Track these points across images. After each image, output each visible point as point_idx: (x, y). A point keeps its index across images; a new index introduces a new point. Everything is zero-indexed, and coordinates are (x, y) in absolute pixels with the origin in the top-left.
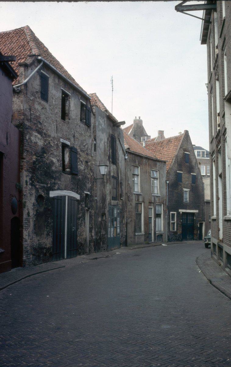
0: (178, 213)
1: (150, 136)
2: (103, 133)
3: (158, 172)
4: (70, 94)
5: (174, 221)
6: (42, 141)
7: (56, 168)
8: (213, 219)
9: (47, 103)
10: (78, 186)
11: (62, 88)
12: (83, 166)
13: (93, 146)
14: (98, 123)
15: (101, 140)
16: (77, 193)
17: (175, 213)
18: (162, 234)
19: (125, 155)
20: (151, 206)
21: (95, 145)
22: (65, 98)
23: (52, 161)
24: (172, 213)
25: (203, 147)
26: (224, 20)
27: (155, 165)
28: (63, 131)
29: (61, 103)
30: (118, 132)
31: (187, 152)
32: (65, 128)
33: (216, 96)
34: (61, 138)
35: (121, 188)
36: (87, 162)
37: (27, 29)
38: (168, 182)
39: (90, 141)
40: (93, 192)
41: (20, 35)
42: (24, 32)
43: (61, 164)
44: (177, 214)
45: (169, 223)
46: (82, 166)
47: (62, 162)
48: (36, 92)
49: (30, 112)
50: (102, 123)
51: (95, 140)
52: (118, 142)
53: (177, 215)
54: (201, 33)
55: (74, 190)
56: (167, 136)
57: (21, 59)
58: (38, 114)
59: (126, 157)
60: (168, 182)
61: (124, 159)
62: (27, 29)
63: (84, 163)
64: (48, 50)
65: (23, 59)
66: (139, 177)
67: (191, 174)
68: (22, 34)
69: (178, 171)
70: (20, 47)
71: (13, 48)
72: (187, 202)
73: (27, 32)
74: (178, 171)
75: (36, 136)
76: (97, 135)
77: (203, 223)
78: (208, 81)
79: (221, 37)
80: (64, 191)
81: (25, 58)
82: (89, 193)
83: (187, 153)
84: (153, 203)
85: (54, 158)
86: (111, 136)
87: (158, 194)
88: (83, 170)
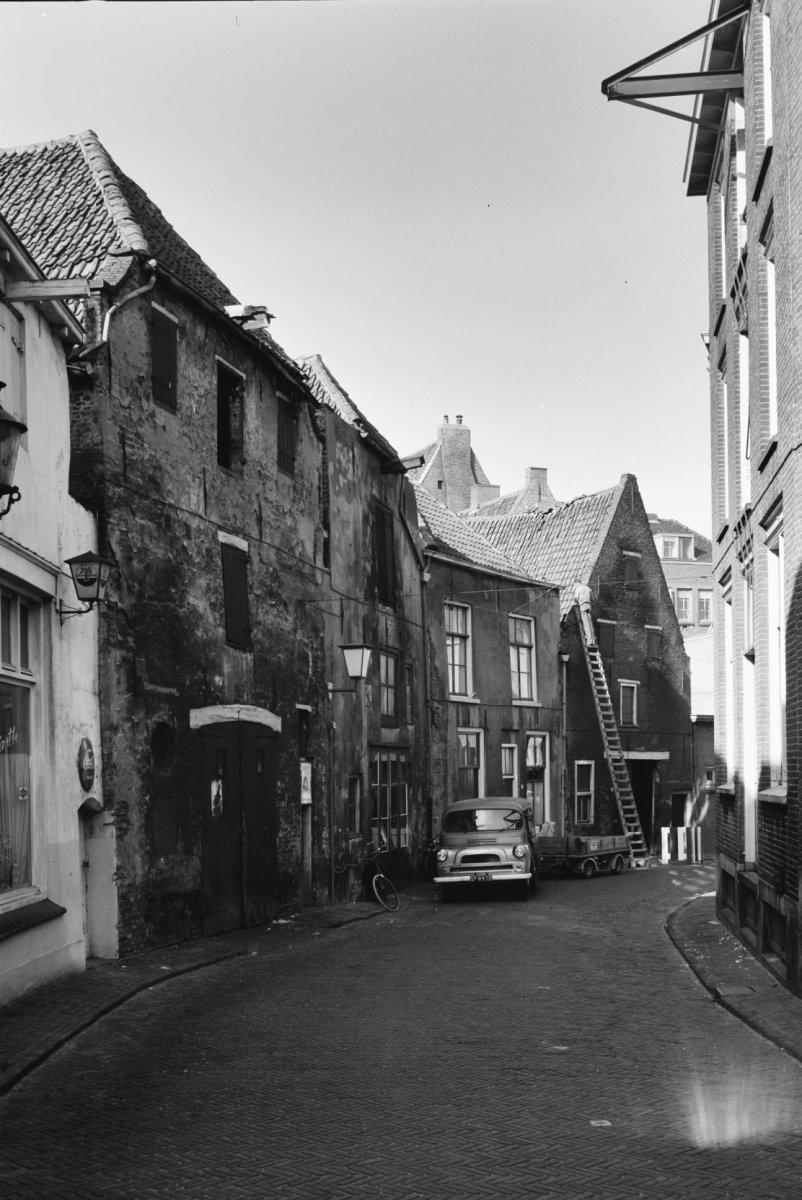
1: (498, 487)
2: (349, 501)
3: (533, 623)
4: (244, 376)
5: (588, 790)
6: (162, 545)
7: (206, 631)
8: (724, 792)
9: (174, 414)
10: (271, 686)
11: (217, 357)
12: (291, 619)
13: (321, 546)
14: (335, 467)
15: (344, 524)
16: (273, 710)
17: (592, 763)
19: (421, 570)
20: (509, 743)
21: (327, 542)
22: (228, 390)
23: (194, 611)
24: (582, 762)
26: (770, 150)
28: (224, 505)
29: (216, 409)
30: (398, 492)
31: (631, 551)
32: (232, 493)
33: (738, 346)
34: (220, 528)
35: (411, 685)
36: (301, 604)
37: (89, 144)
38: (566, 658)
39: (306, 532)
40: (321, 705)
41: (66, 164)
42: (78, 155)
43: (221, 616)
44: (596, 765)
45: (570, 801)
46: (286, 620)
47: (224, 609)
48: (139, 377)
49: (123, 448)
50: (348, 463)
51: (326, 526)
52: (398, 527)
53: (595, 769)
54: (688, 155)
55: (263, 701)
56: (562, 491)
57: (83, 262)
59: (427, 577)
60: (566, 658)
61: (418, 582)
62: (89, 144)
63: (291, 608)
64: (159, 212)
65: (90, 261)
66: (469, 642)
67: (646, 626)
68: (73, 161)
70: (72, 215)
71: (45, 218)
72: (632, 723)
73: (92, 155)
75: (142, 526)
76: (333, 509)
78: (711, 326)
79: (756, 197)
80: (234, 706)
81: (96, 260)
82: (308, 708)
83: (632, 554)
84: (517, 731)
85: (201, 600)
86: (378, 509)
87: (531, 699)
88: (289, 633)
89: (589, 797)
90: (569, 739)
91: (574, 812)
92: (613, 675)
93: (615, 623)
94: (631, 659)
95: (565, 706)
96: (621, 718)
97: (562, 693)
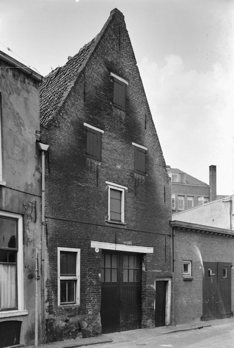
0: (88, 253)
5: (74, 273)
17: (78, 251)
18: (18, 319)
25: (93, 38)
27: (199, 188)
58: (118, 61)
67: (133, 144)
69: (85, 124)
72: (120, 221)
74: (85, 124)
77: (168, 281)
89: (76, 281)
90: (49, 226)
91: (57, 296)
92: (101, 177)
93: (103, 132)
94: (119, 167)
95: (43, 194)
96: (109, 215)
97: (40, 181)
